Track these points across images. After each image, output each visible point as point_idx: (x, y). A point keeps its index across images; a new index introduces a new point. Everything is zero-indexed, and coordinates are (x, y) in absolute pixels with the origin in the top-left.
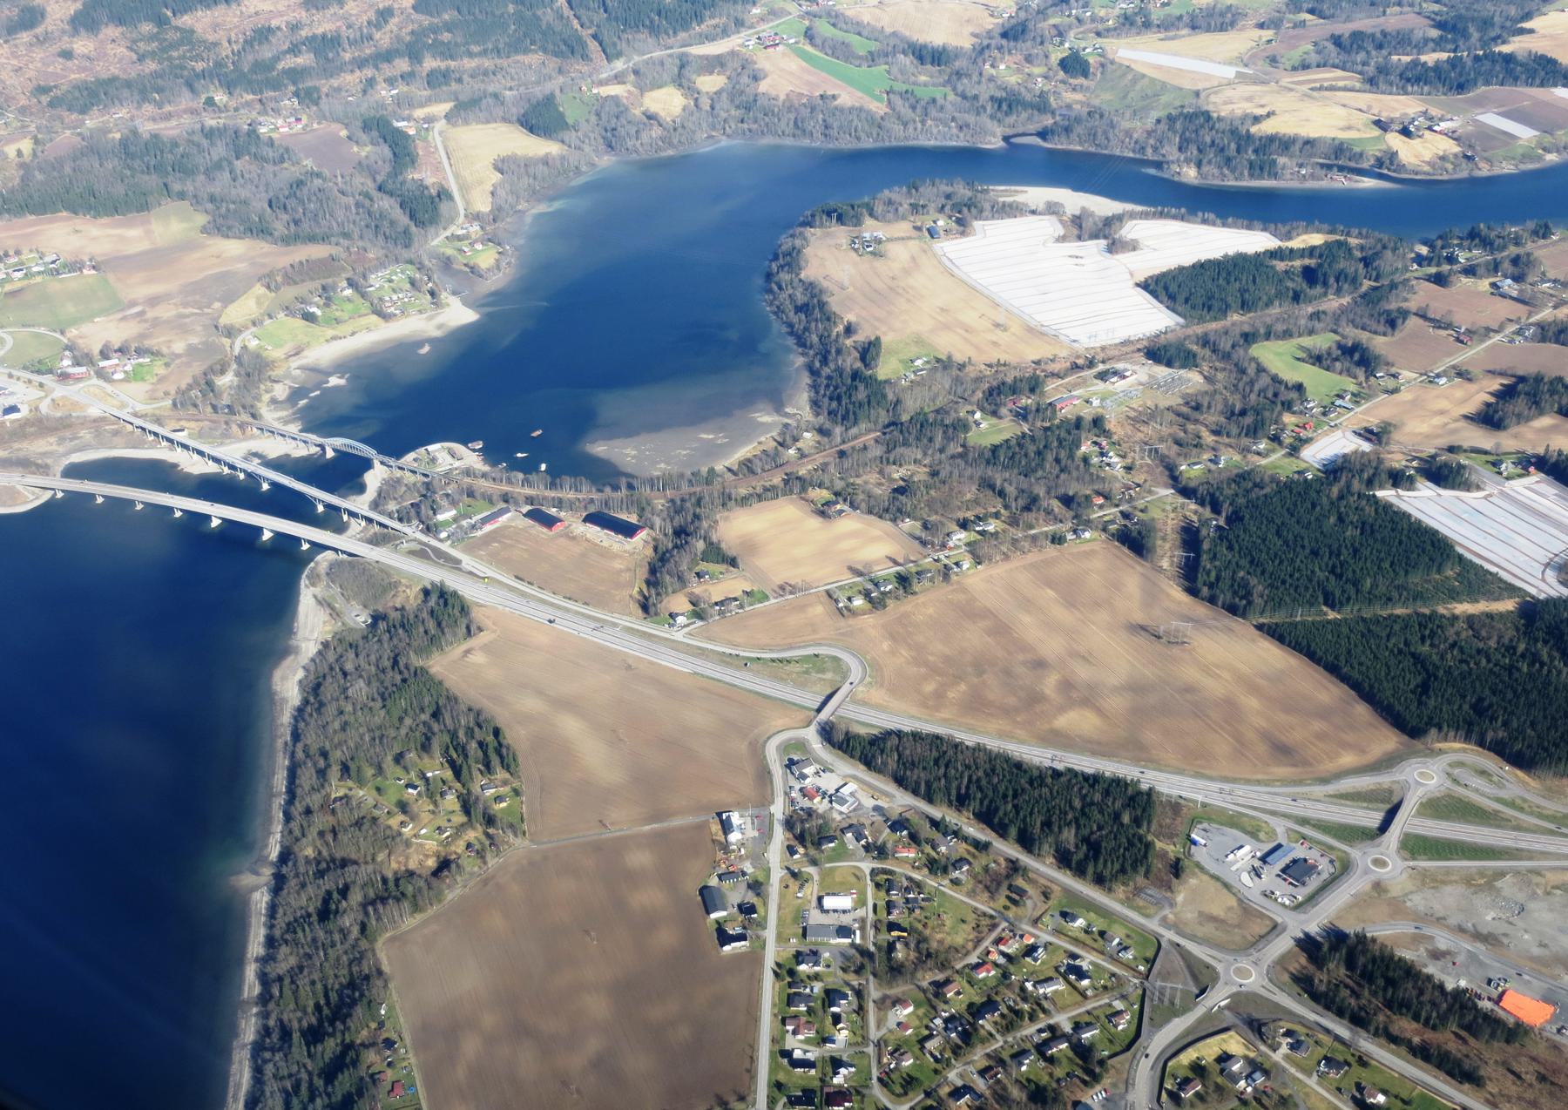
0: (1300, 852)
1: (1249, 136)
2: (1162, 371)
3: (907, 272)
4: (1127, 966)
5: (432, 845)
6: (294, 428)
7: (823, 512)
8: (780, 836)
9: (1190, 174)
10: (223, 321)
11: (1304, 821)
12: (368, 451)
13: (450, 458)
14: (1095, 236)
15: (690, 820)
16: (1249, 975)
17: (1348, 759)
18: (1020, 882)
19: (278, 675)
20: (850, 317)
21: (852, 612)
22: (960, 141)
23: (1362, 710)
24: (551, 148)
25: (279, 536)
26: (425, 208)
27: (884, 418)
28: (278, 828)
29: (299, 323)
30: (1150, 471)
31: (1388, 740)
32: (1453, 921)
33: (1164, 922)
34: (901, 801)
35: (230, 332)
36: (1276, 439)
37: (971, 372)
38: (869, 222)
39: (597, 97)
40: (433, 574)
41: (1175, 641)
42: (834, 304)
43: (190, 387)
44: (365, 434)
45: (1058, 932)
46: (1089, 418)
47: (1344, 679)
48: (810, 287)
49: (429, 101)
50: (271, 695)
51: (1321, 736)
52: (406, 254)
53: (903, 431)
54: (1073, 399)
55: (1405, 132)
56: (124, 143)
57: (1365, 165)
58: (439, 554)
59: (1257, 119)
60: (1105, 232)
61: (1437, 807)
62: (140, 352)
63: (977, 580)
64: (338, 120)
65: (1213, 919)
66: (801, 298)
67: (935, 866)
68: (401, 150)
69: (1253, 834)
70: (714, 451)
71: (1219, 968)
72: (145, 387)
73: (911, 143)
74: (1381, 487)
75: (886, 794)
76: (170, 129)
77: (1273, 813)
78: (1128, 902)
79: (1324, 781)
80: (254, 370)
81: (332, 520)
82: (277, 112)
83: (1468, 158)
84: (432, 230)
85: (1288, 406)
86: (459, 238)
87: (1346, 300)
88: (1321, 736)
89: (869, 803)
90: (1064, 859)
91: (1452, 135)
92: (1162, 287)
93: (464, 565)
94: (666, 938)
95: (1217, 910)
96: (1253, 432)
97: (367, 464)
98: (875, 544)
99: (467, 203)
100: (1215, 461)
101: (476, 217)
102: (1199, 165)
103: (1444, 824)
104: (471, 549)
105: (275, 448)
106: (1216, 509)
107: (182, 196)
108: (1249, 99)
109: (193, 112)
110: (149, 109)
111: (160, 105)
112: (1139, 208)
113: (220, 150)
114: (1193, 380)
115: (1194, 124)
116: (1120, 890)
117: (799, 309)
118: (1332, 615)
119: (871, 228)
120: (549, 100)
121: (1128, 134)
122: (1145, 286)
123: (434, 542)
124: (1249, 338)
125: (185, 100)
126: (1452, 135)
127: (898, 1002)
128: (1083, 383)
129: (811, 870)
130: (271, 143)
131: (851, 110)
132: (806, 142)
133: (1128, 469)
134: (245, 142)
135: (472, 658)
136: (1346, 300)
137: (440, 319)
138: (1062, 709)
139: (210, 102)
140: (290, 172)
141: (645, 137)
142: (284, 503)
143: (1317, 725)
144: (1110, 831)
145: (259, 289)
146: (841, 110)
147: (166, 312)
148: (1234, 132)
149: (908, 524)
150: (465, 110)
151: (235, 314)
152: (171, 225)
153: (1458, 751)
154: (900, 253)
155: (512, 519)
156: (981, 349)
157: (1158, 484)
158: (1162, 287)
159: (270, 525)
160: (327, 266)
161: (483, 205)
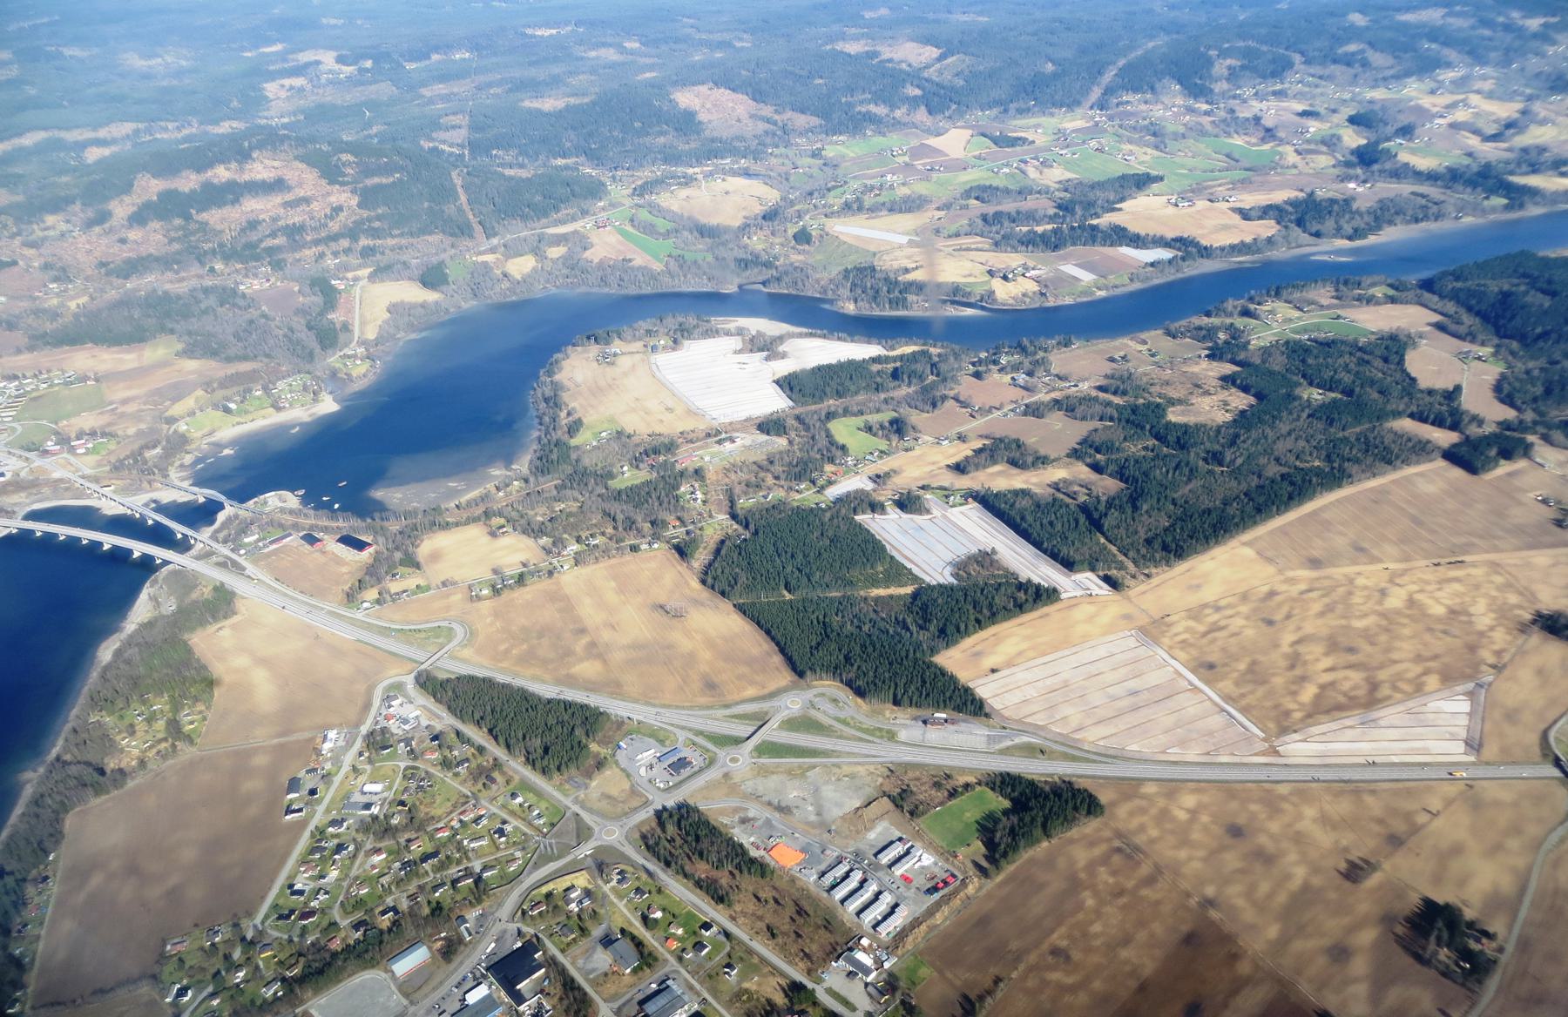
0: (686, 753)
1: (897, 282)
2: (764, 437)
3: (625, 374)
4: (538, 829)
5: (136, 752)
6: (185, 484)
7: (493, 534)
8: (359, 744)
9: (850, 308)
10: (169, 413)
11: (700, 733)
12: (221, 498)
13: (280, 501)
14: (761, 350)
15: (307, 735)
16: (613, 834)
17: (751, 692)
18: (496, 775)
19: (104, 645)
20: (572, 405)
21: (479, 598)
22: (707, 288)
23: (777, 659)
24: (431, 296)
25: (115, 548)
26: (329, 337)
27: (569, 470)
28: (641, 861)
29: (220, 413)
30: (719, 503)
31: (786, 677)
32: (766, 799)
33: (576, 801)
34: (445, 720)
35: (171, 421)
36: (813, 482)
37: (636, 440)
38: (617, 342)
39: (474, 263)
40: (220, 576)
41: (678, 615)
42: (565, 396)
43: (127, 457)
44: (228, 486)
45: (504, 806)
46: (691, 470)
47: (773, 639)
48: (557, 387)
49: (359, 267)
50: (94, 657)
51: (740, 677)
52: (308, 367)
53: (580, 477)
54: (686, 459)
55: (1005, 278)
56: (147, 297)
57: (972, 300)
58: (235, 564)
59: (907, 271)
60: (768, 347)
61: (792, 724)
62: (104, 434)
63: (571, 578)
64: (293, 280)
65: (609, 797)
66: (548, 392)
67: (446, 764)
68: (330, 297)
69: (662, 742)
70: (456, 493)
71: (596, 829)
72: (97, 457)
73: (677, 290)
74: (864, 512)
75: (438, 717)
76: (181, 288)
77: (678, 727)
78: (559, 788)
79: (727, 706)
80: (179, 443)
81: (183, 546)
82: (256, 276)
83: (1042, 294)
84: (330, 351)
85: (831, 460)
86: (349, 357)
87: (911, 390)
88: (740, 677)
89: (424, 723)
90: (530, 761)
91: (1037, 280)
92: (789, 384)
93: (247, 572)
94: (253, 811)
95: (614, 791)
96: (799, 477)
97: (221, 507)
98: (515, 551)
99: (362, 332)
100: (765, 497)
101: (363, 343)
102: (856, 301)
103: (793, 735)
104: (255, 562)
105: (167, 496)
106: (747, 527)
107: (172, 332)
108: (909, 257)
109: (200, 277)
110: (169, 275)
111: (177, 272)
112: (805, 330)
113: (212, 301)
114: (781, 442)
115: (864, 277)
116: (557, 777)
117: (546, 400)
118: (788, 596)
119: (617, 346)
120: (441, 264)
121: (818, 281)
122: (777, 382)
123: (234, 556)
124: (830, 416)
125: (196, 269)
126: (1037, 280)
127: (378, 851)
128: (707, 446)
129: (368, 767)
130: (244, 296)
131: (640, 268)
132: (606, 290)
133: (704, 502)
134: (228, 296)
135: (221, 633)
136: (911, 390)
137: (314, 410)
138: (581, 660)
139: (212, 270)
140: (253, 313)
141: (497, 289)
142: (159, 536)
143: (743, 669)
144: (558, 735)
145: (200, 393)
146: (632, 269)
147: (131, 408)
148: (886, 279)
149: (545, 540)
150: (382, 272)
151: (177, 409)
152: (156, 351)
153: (828, 687)
154: (624, 362)
155: (294, 540)
156: (640, 425)
157: (720, 512)
158: (789, 384)
159: (138, 548)
160: (251, 377)
161: (371, 335)
